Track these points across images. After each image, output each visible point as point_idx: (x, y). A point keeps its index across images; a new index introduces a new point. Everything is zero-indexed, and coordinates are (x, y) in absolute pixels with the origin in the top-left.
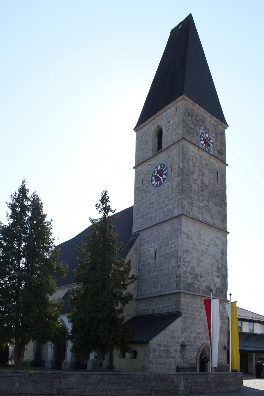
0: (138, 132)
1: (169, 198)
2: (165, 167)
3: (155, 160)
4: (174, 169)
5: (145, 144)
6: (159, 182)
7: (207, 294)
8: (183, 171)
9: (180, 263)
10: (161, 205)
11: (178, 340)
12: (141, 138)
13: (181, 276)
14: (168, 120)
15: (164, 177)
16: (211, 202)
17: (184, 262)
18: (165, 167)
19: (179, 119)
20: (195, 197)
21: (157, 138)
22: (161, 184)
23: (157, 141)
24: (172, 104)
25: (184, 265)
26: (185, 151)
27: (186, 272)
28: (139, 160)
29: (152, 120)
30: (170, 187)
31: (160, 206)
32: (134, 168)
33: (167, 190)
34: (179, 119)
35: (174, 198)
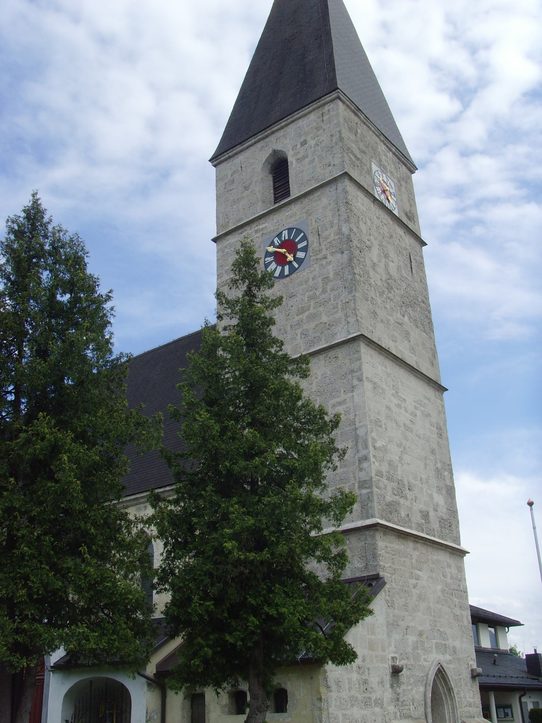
0: (221, 166)
1: (318, 300)
2: (302, 234)
3: (273, 220)
4: (326, 238)
5: (243, 188)
6: (287, 268)
7: (425, 531)
8: (351, 241)
9: (364, 452)
10: (297, 318)
11: (383, 653)
12: (229, 177)
13: (373, 482)
14: (302, 140)
15: (301, 255)
16: (406, 317)
17: (374, 447)
18: (302, 234)
19: (330, 136)
20: (379, 300)
21: (272, 178)
22: (293, 270)
23: (271, 183)
24: (307, 110)
25: (374, 456)
26: (351, 200)
27: (379, 474)
28: (228, 222)
29: (259, 141)
30: (319, 277)
31: (294, 320)
32: (215, 240)
33: (311, 283)
34: (331, 136)
35: (332, 300)
